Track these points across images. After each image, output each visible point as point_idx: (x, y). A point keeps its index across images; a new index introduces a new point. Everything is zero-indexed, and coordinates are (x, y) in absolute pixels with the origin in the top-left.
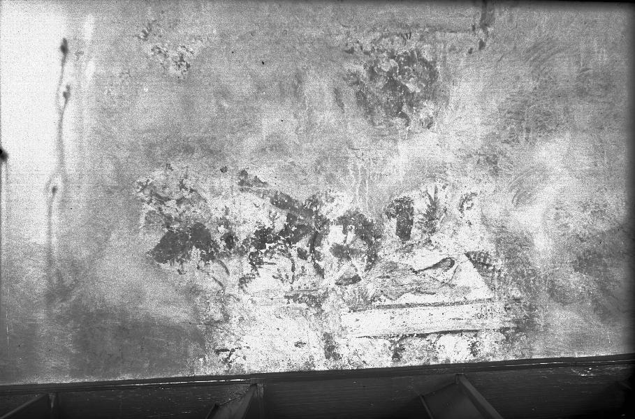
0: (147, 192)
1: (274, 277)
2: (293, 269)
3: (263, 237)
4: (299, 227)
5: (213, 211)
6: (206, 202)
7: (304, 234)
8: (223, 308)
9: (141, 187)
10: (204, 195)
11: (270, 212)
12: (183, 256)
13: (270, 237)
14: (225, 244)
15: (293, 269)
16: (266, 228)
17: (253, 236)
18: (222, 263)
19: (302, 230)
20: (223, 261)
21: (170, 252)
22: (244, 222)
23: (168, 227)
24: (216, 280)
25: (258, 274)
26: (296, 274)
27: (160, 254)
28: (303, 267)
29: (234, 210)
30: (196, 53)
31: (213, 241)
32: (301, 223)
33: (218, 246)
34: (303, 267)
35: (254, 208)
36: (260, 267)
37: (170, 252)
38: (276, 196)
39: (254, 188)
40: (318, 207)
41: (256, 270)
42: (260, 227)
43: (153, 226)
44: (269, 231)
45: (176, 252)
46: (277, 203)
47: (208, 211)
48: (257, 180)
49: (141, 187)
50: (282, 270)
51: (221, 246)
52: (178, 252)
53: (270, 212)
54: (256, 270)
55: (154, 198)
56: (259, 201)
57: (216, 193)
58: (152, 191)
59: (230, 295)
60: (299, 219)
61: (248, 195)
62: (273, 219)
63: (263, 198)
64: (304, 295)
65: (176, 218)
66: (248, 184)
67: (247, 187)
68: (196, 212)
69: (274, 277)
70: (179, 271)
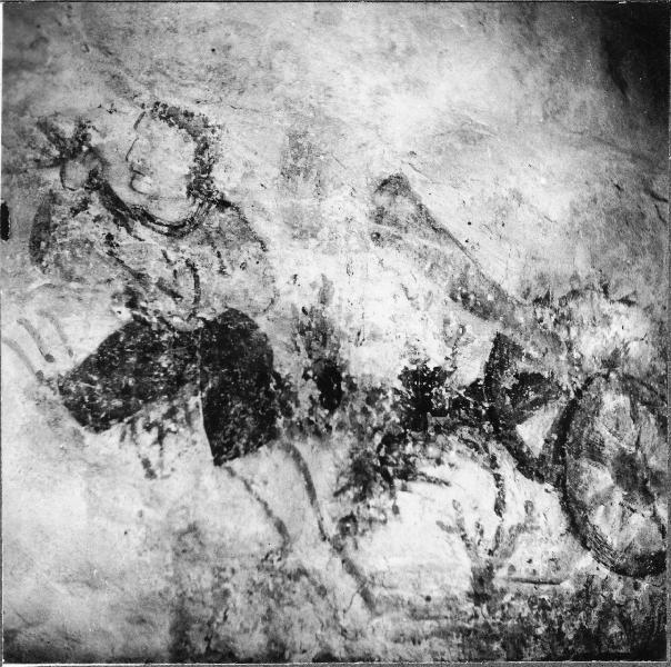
0: (78, 172)
1: (440, 524)
2: (499, 508)
3: (425, 403)
4: (525, 379)
5: (282, 283)
6: (264, 248)
7: (537, 403)
8: (268, 617)
9: (56, 153)
10: (261, 226)
11: (447, 322)
12: (171, 414)
13: (439, 396)
14: (317, 393)
15: (499, 508)
16: (431, 366)
17: (398, 385)
18: (297, 457)
19: (536, 391)
20: (299, 446)
21: (125, 392)
22: (374, 336)
23: (132, 305)
24: (269, 513)
25: (396, 510)
26: (506, 526)
27: (90, 391)
28: (529, 506)
29: (343, 292)
30: (169, 361)
31: (277, 376)
32: (531, 369)
33: (294, 396)
34: (529, 506)
35: (403, 301)
36: (404, 489)
37: (125, 392)
38: (463, 281)
39: (413, 239)
40: (574, 331)
41: (392, 496)
42: (415, 362)
43: (79, 291)
44: (438, 376)
45: (147, 395)
46: (465, 297)
47: (267, 280)
48: (425, 218)
49: (56, 153)
50: (466, 506)
51: (303, 397)
52: (155, 396)
53: (447, 322)
54: (392, 496)
55: (95, 196)
56: (420, 285)
57: (302, 230)
58: (93, 174)
59: (302, 572)
60: (528, 356)
61: (389, 254)
62: (454, 342)
63: (429, 274)
64: (518, 595)
65: (160, 285)
66: (395, 223)
67: (392, 230)
68: (229, 285)
69: (440, 524)
70: (146, 464)
